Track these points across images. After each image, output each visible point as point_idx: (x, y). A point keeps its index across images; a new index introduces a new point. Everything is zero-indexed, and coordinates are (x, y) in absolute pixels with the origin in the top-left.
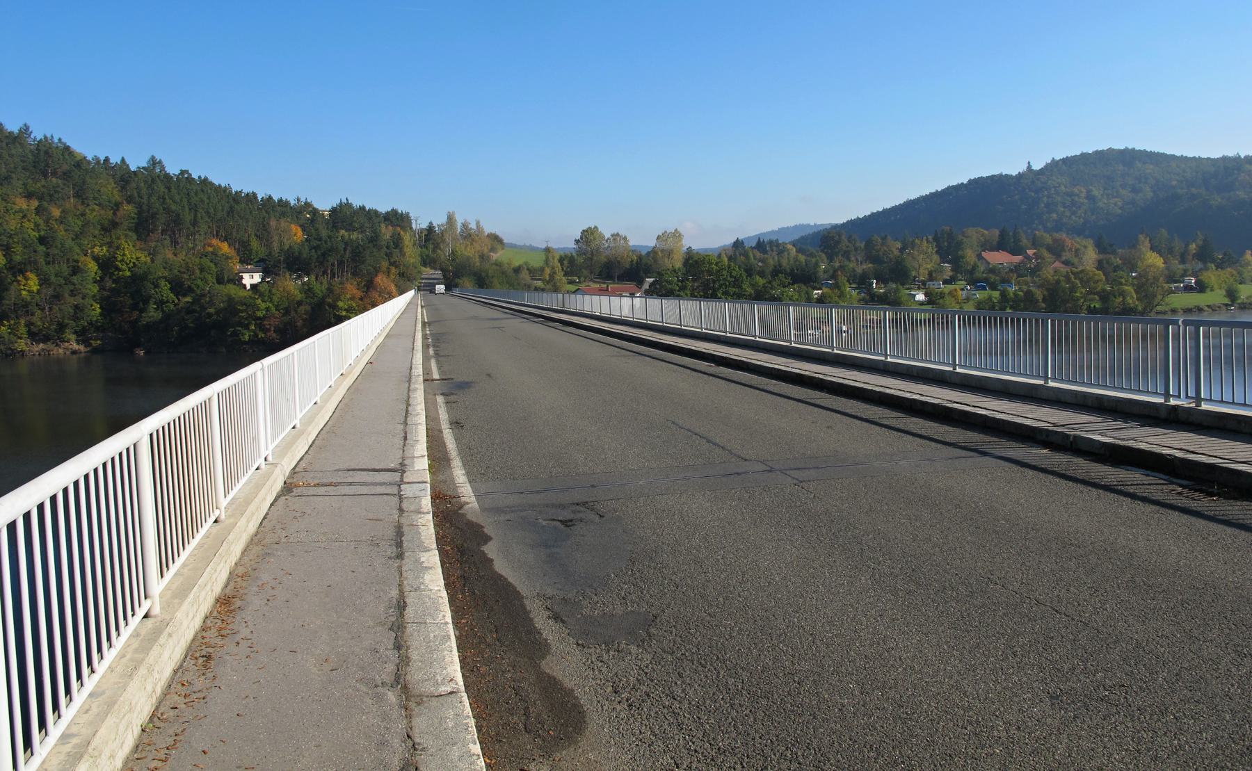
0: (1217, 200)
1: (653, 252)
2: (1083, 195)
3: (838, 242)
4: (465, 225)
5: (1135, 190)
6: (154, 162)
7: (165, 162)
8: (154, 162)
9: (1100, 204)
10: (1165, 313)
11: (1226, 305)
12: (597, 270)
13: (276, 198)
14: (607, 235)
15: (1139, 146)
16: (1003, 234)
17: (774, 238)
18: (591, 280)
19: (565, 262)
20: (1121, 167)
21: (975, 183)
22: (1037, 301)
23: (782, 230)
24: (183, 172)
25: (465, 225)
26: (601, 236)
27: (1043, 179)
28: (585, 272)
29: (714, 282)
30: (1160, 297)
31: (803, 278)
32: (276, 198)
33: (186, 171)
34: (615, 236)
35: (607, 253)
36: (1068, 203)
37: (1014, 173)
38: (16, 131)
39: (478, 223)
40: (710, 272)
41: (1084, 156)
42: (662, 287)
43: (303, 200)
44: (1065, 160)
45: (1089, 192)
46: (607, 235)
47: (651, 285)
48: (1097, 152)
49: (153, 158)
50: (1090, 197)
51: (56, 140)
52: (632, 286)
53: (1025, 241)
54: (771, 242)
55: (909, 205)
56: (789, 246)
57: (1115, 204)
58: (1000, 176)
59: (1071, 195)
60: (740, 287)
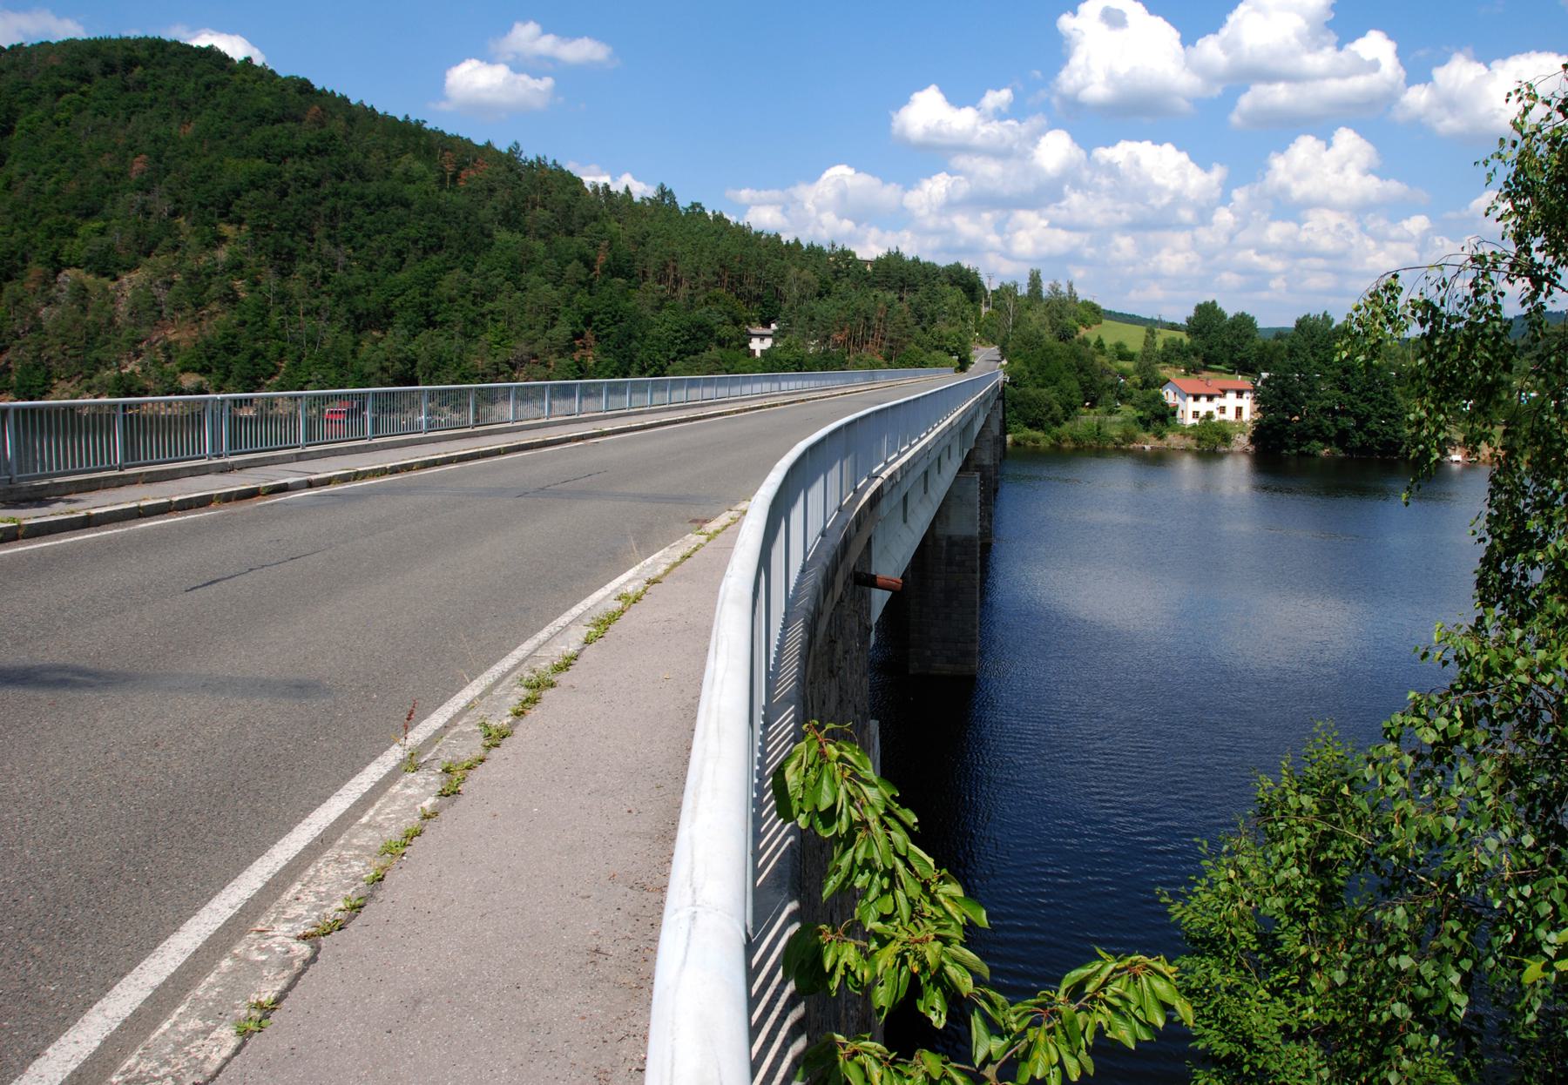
4: (1055, 289)
6: (664, 193)
7: (676, 193)
8: (664, 193)
13: (683, 202)
24: (694, 205)
25: (1055, 289)
32: (683, 202)
33: (699, 205)
38: (505, 150)
39: (1070, 286)
43: (839, 247)
49: (662, 187)
51: (550, 162)
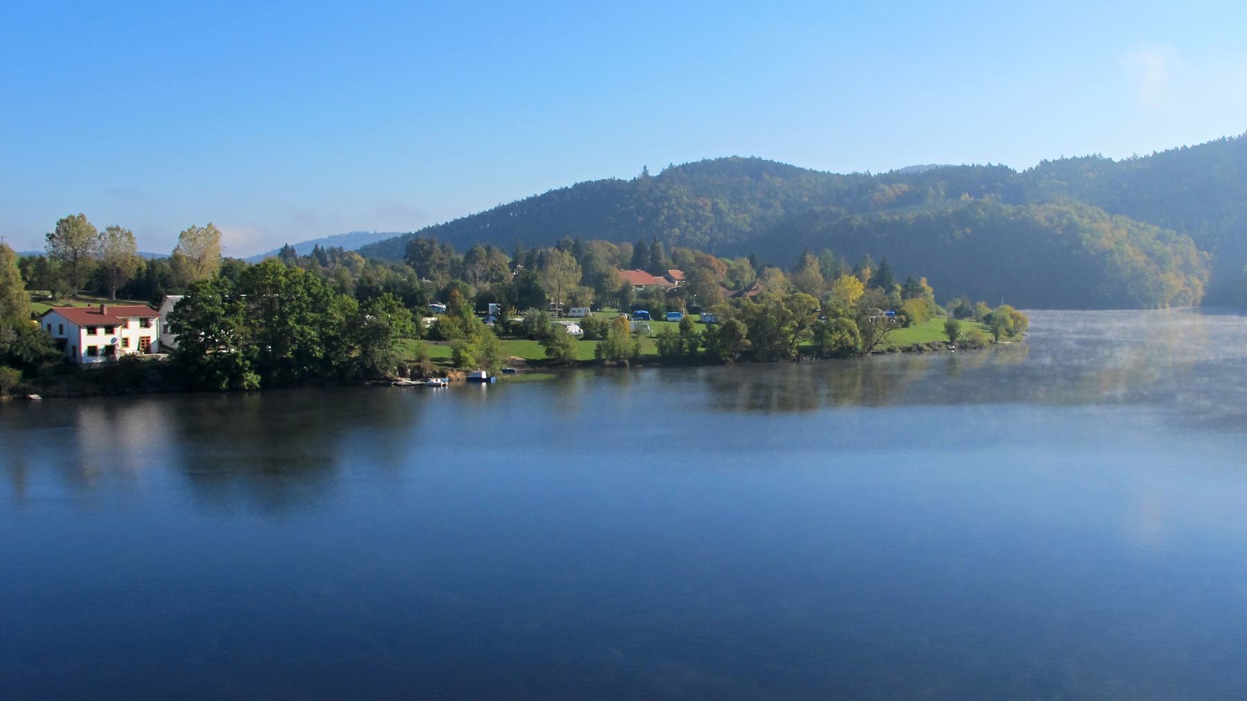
0: (858, 220)
1: (175, 260)
2: (709, 208)
3: (429, 253)
5: (763, 205)
9: (728, 220)
10: (882, 353)
11: (946, 343)
12: (83, 281)
14: (101, 229)
15: (766, 157)
16: (639, 249)
17: (336, 246)
18: (74, 297)
19: (30, 268)
20: (748, 179)
21: (583, 189)
22: (740, 336)
23: (351, 237)
26: (91, 231)
27: (663, 186)
28: (63, 284)
29: (282, 302)
30: (879, 332)
31: (1160, 398)
34: (113, 230)
35: (96, 258)
36: (691, 217)
37: (629, 178)
40: (276, 287)
41: (706, 164)
42: (196, 309)
44: (685, 167)
45: (714, 204)
46: (101, 229)
47: (179, 305)
48: (720, 160)
50: (716, 211)
52: (143, 306)
53: (664, 259)
54: (332, 251)
55: (502, 211)
56: (357, 257)
57: (744, 220)
58: (612, 181)
59: (695, 207)
60: (323, 311)
